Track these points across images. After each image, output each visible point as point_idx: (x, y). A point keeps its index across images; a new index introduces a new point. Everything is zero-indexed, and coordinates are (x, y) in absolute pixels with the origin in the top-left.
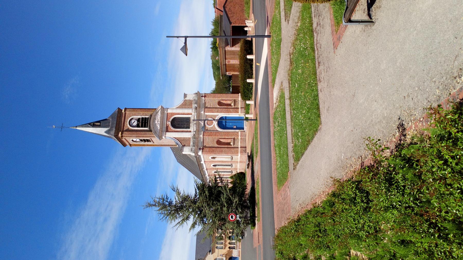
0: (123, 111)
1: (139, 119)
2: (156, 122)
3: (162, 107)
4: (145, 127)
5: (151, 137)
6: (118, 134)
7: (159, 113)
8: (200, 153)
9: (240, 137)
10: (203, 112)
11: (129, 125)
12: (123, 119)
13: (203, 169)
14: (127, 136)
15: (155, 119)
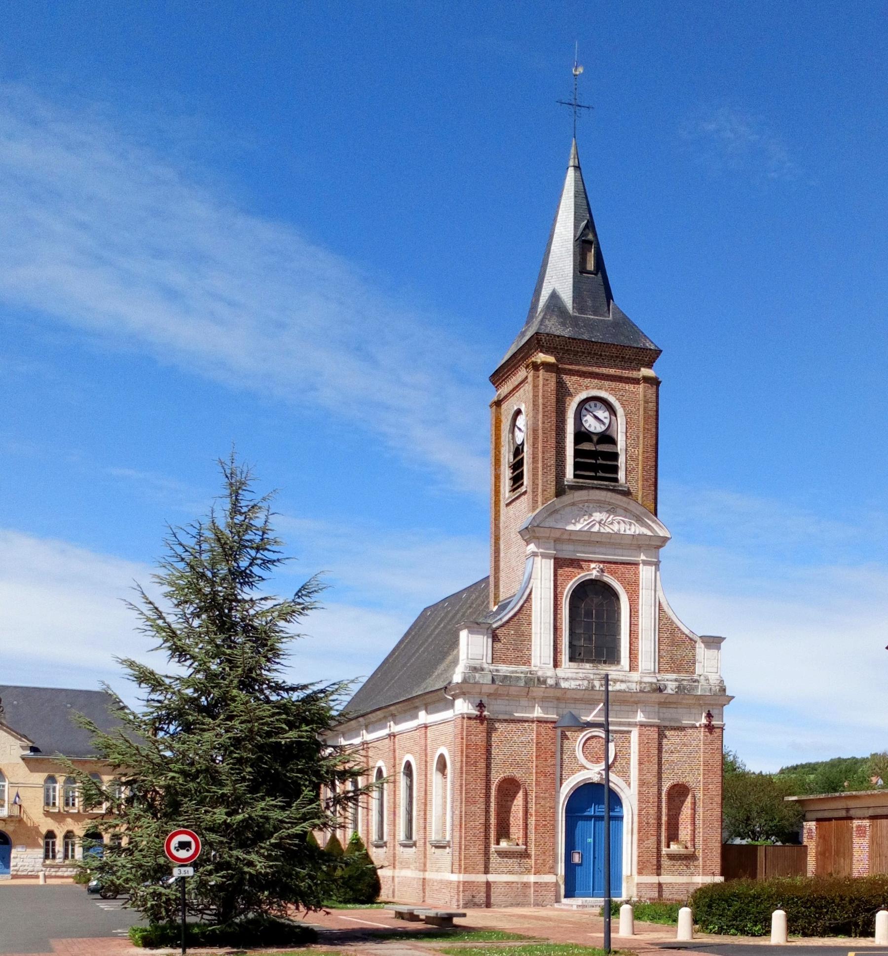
0: (645, 372)
1: (613, 441)
2: (597, 516)
3: (665, 540)
4: (577, 466)
7: (636, 529)
8: (463, 707)
9: (532, 878)
10: (640, 717)
11: (583, 395)
12: (612, 371)
14: (535, 386)
15: (612, 509)
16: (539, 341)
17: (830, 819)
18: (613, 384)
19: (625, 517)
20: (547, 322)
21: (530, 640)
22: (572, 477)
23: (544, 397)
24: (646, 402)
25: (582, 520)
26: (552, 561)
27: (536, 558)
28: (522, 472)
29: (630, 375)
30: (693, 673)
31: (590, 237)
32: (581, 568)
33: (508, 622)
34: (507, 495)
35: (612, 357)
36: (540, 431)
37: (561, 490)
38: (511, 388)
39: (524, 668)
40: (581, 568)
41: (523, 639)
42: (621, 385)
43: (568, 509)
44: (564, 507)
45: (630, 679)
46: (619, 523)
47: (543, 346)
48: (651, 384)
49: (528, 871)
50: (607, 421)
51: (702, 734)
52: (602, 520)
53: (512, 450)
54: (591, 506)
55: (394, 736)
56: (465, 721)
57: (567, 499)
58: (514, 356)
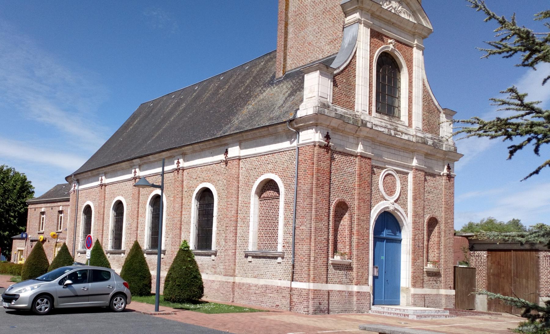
8: (311, 136)
9: (355, 288)
10: (415, 163)
13: (185, 156)
17: (510, 250)
21: (354, 89)
26: (369, 29)
30: (439, 135)
32: (383, 41)
33: (342, 71)
39: (350, 112)
40: (383, 41)
41: (351, 87)
45: (409, 133)
49: (350, 282)
51: (444, 180)
55: (183, 170)
56: (316, 148)
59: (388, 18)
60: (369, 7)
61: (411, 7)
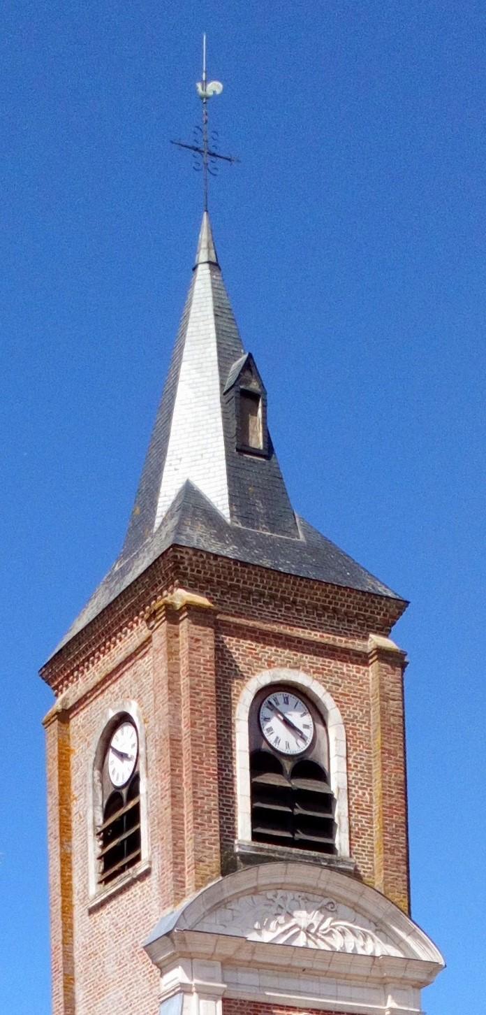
0: (376, 640)
1: (320, 774)
2: (303, 917)
3: (433, 968)
4: (258, 817)
5: (177, 862)
6: (194, 585)
7: (376, 947)
11: (264, 678)
12: (315, 636)
14: (172, 654)
15: (329, 906)
16: (177, 563)
18: (319, 661)
19: (353, 922)
20: (188, 531)
22: (248, 837)
23: (192, 673)
24: (385, 698)
25: (273, 925)
26: (220, 1003)
27: (187, 997)
28: (138, 833)
29: (350, 646)
31: (254, 386)
34: (93, 888)
35: (315, 608)
36: (186, 744)
37: (229, 866)
38: (98, 677)
42: (334, 665)
43: (246, 900)
44: (237, 896)
46: (343, 933)
47: (185, 575)
48: (393, 665)
50: (308, 734)
52: (311, 925)
53: (101, 801)
54: (290, 896)
57: (245, 878)
58: (109, 609)
59: (285, 962)
60: (209, 949)
61: (366, 911)
